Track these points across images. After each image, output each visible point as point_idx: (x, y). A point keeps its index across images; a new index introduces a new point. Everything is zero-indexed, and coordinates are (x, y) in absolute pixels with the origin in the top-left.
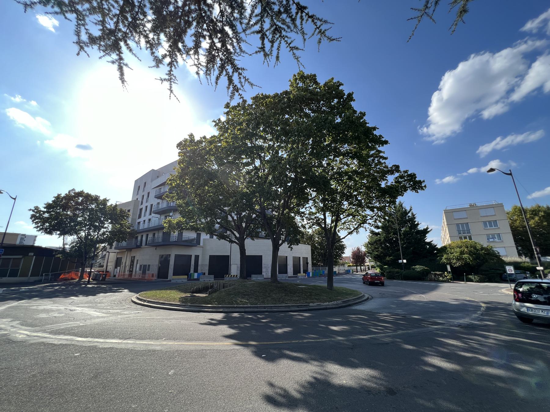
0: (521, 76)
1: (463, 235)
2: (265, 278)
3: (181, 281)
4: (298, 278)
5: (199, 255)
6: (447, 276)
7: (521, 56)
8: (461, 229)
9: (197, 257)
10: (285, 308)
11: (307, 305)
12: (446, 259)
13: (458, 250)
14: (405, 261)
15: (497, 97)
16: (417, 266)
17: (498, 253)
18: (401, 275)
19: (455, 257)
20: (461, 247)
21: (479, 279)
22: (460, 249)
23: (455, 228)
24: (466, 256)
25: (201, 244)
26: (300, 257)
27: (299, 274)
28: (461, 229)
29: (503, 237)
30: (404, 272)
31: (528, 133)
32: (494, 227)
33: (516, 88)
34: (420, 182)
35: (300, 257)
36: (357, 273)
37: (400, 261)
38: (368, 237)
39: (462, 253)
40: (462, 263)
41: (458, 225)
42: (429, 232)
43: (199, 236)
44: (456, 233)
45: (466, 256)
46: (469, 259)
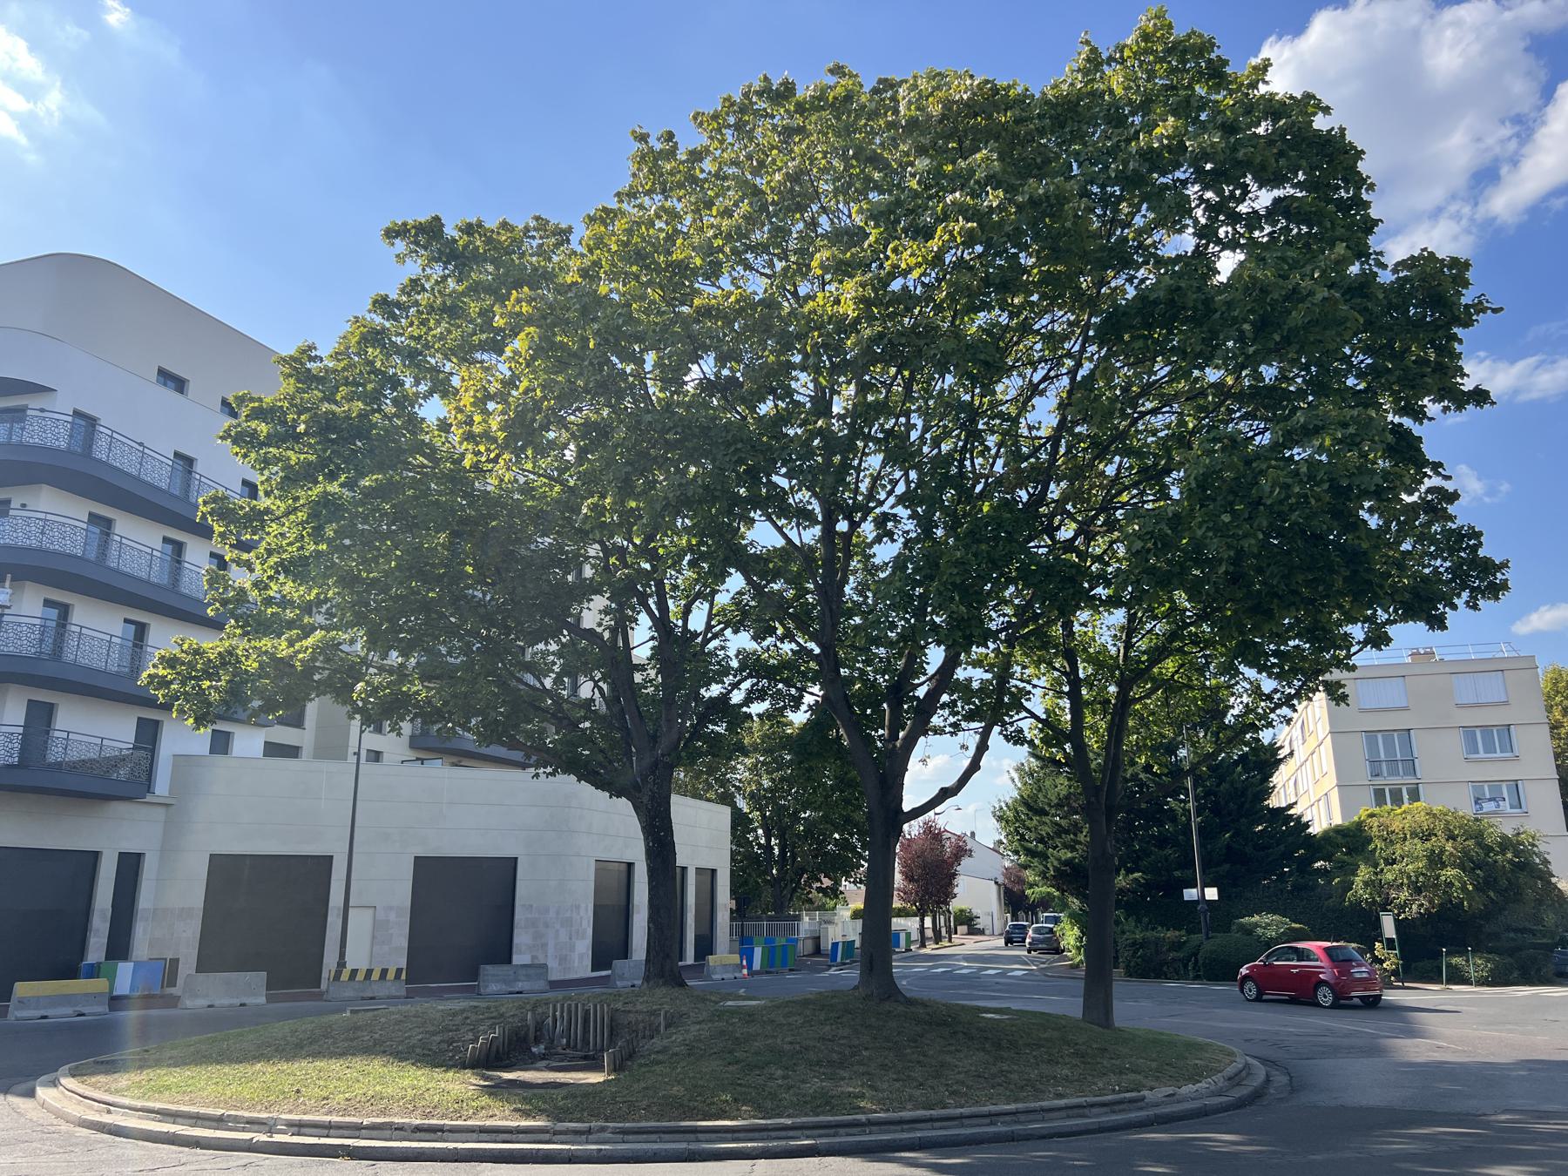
0: (1525, 126)
1: (1388, 781)
2: (555, 985)
3: (69, 1011)
4: (709, 978)
5: (516, 859)
6: (1381, 962)
7: (1522, 45)
8: (1383, 756)
9: (130, 865)
10: (1068, 1117)
11: (1131, 1101)
12: (1366, 884)
13: (1419, 847)
14: (1212, 894)
15: (1435, 195)
16: (1267, 918)
17: (1546, 862)
18: (1195, 955)
19: (1409, 877)
20: (1426, 836)
21: (1491, 970)
22: (1428, 845)
23: (1359, 746)
24: (1450, 873)
25: (162, 786)
26: (714, 872)
27: (617, 963)
28: (1383, 756)
29: (1529, 792)
30: (1208, 946)
31: (1532, 360)
32: (1499, 754)
33: (1504, 170)
34: (1488, 567)
35: (714, 872)
36: (923, 951)
37: (1191, 894)
38: (1015, 776)
39: (1436, 860)
40: (1431, 901)
41: (1371, 735)
42: (1281, 760)
43: (148, 734)
44: (1362, 774)
45: (1450, 873)
46: (1464, 889)
